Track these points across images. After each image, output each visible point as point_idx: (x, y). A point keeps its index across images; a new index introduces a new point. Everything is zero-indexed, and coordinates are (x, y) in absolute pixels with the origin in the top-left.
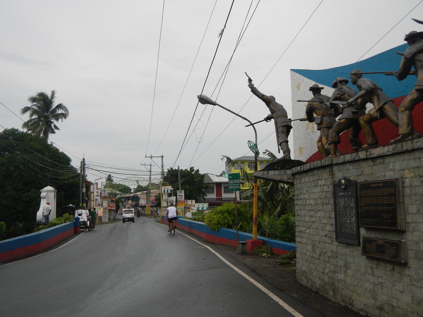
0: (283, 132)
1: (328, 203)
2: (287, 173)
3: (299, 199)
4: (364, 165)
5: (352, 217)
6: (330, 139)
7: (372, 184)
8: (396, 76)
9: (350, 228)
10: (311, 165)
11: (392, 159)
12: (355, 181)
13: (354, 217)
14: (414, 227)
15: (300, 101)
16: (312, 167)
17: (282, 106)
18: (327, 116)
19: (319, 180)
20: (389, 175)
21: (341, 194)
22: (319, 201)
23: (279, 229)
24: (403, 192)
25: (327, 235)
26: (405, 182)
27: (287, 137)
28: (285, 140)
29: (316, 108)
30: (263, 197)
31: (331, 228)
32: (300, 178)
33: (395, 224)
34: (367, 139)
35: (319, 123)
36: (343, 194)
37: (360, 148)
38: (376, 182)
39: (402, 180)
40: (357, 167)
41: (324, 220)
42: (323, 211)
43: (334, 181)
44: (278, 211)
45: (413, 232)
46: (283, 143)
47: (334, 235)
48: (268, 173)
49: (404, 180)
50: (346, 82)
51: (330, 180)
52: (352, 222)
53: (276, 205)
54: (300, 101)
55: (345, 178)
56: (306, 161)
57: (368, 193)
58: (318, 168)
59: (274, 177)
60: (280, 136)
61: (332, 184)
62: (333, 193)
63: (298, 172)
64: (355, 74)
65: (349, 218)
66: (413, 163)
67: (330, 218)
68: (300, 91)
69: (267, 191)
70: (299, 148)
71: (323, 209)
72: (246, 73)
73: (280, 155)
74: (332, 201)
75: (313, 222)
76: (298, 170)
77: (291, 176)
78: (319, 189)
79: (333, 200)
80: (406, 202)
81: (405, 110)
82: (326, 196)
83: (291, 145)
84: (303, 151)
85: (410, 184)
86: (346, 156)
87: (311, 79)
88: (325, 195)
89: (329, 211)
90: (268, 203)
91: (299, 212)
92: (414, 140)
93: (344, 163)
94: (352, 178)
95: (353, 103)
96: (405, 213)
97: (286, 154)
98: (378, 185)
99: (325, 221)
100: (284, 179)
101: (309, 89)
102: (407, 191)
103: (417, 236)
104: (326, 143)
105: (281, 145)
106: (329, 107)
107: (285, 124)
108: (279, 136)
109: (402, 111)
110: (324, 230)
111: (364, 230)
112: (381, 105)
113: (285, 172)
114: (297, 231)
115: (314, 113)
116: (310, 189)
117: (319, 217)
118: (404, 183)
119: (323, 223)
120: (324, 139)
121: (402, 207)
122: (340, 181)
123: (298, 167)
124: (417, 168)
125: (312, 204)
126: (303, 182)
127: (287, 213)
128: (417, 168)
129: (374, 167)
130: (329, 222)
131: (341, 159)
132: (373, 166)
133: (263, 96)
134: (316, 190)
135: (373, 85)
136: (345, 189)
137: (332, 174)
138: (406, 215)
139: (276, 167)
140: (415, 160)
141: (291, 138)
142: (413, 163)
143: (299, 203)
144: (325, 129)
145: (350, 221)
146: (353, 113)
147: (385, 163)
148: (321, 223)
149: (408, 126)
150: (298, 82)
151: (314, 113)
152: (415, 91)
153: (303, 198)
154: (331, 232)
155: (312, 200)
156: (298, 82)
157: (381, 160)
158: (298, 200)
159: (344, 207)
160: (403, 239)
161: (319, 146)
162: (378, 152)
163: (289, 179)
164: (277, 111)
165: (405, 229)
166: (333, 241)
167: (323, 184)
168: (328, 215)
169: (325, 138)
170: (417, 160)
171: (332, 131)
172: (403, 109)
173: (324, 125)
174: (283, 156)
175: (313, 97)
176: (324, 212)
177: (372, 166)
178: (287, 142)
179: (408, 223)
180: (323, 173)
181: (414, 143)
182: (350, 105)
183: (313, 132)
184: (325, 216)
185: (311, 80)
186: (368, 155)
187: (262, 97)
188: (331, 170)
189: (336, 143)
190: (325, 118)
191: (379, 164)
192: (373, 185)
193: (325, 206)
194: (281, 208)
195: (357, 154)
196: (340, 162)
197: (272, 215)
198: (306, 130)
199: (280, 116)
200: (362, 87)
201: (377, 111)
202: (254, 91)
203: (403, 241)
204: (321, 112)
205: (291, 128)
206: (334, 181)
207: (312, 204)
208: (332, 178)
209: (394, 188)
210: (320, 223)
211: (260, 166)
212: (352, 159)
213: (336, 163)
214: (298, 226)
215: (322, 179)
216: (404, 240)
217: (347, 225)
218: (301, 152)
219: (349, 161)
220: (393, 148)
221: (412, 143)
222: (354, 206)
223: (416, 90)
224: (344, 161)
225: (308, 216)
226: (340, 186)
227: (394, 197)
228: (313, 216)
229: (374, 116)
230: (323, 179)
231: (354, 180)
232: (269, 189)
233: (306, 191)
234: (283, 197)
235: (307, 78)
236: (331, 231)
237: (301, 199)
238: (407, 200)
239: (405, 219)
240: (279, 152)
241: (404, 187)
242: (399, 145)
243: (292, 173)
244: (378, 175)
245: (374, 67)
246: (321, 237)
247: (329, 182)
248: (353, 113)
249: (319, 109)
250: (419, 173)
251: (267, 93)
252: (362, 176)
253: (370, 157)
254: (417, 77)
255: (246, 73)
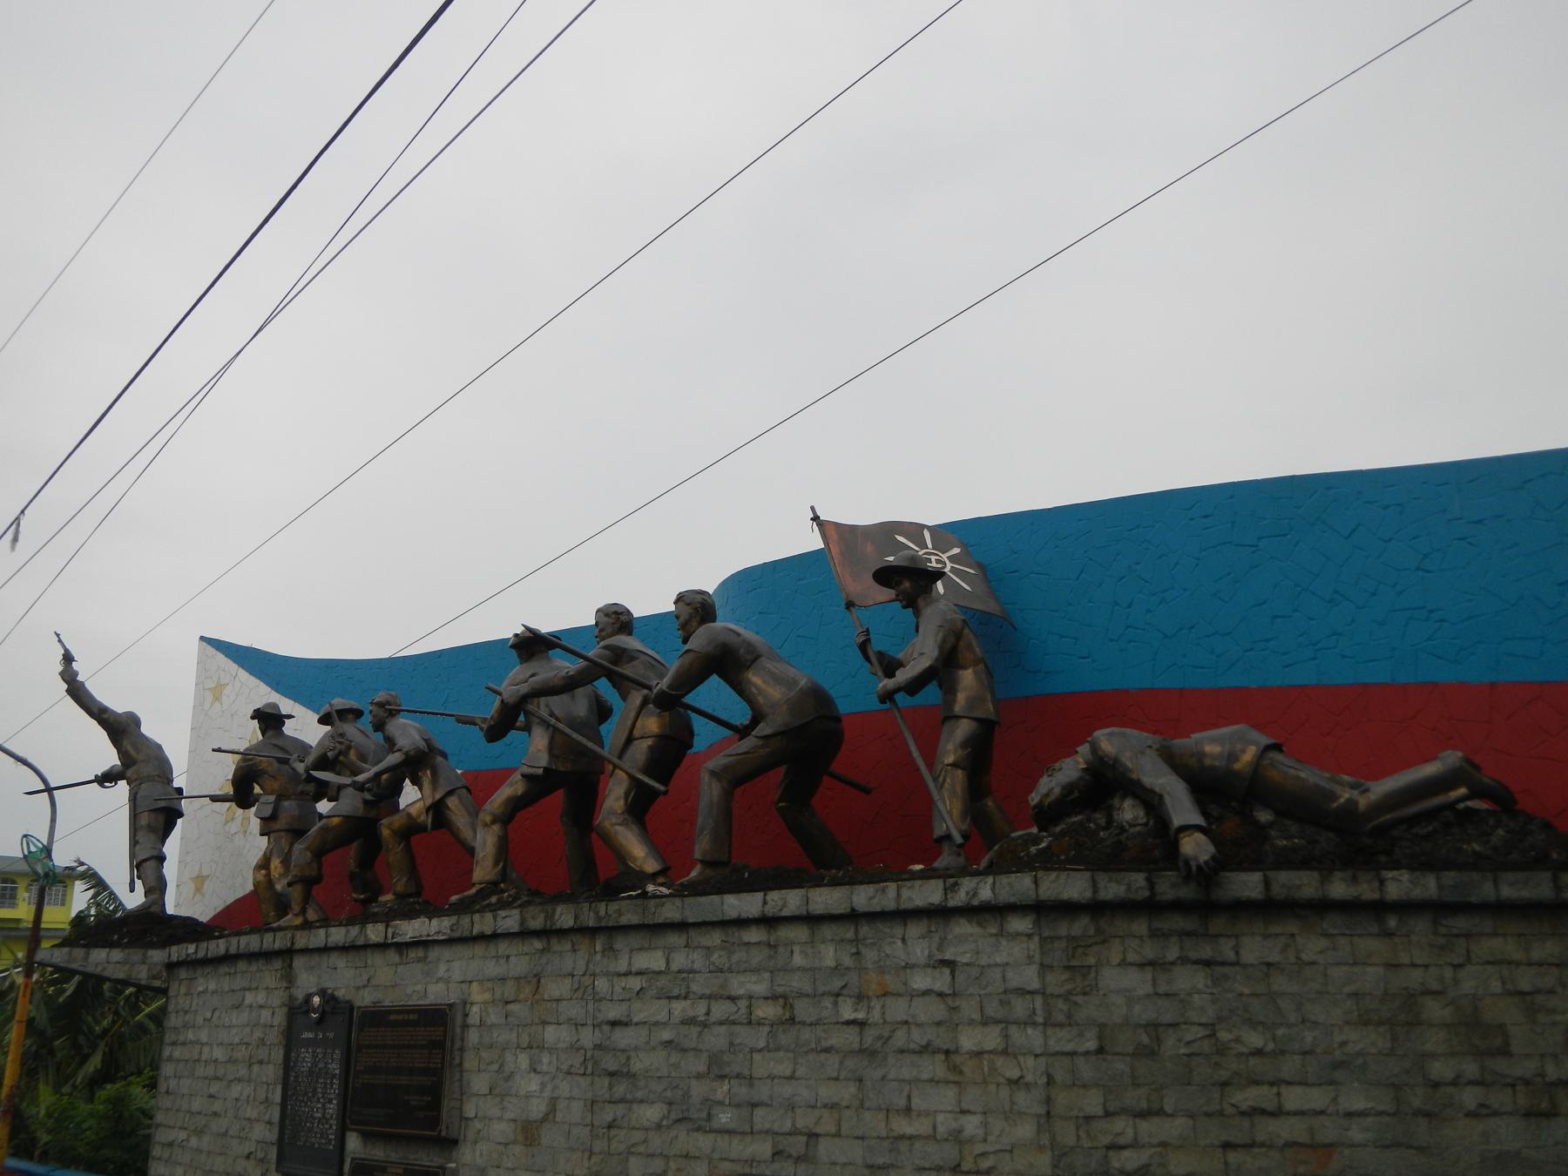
0: (150, 828)
1: (266, 1060)
2: (151, 957)
3: (179, 1042)
4: (376, 959)
5: (330, 1101)
6: (294, 872)
7: (389, 1012)
8: (481, 729)
9: (321, 1134)
10: (230, 944)
11: (446, 953)
12: (348, 1002)
13: (334, 1102)
14: (480, 1131)
15: (219, 750)
16: (233, 951)
17: (159, 747)
18: (293, 797)
19: (249, 989)
20: (436, 993)
21: (306, 1035)
22: (242, 1053)
23: (88, 1133)
24: (463, 1040)
25: (251, 1153)
26: (471, 1013)
27: (163, 843)
28: (155, 853)
29: (266, 773)
30: (42, 1019)
31: (267, 1133)
32: (191, 979)
33: (435, 1122)
34: (394, 881)
35: (267, 816)
36: (311, 1035)
37: (374, 904)
38: (399, 1010)
39: (464, 1007)
40: (359, 965)
41: (249, 1110)
42: (248, 1082)
43: (291, 997)
44: (91, 1069)
45: (476, 1142)
46: (148, 863)
47: (273, 1154)
48: (88, 954)
49: (467, 1009)
50: (358, 714)
51: (281, 993)
52: (328, 1116)
53: (86, 1051)
54: (219, 750)
55: (322, 992)
56: (209, 921)
57: (379, 1038)
58: (252, 957)
59: (104, 969)
60: (140, 841)
61: (286, 1005)
62: (284, 1030)
63: (189, 959)
64: (381, 705)
65: (319, 1106)
66: (493, 969)
67: (266, 1105)
68: (222, 704)
69: (61, 1000)
70: (195, 876)
71: (250, 1076)
72: (58, 635)
73: (133, 899)
74: (278, 1055)
75: (215, 1114)
76: (188, 955)
77: (163, 969)
78: (244, 1016)
79: (282, 1052)
80: (467, 1065)
81: (493, 822)
82: (263, 1039)
83: (170, 870)
84: (207, 886)
85: (481, 1021)
86: (333, 930)
87: (259, 678)
88: (261, 1036)
89: (266, 1083)
90: (60, 1041)
91: (173, 1083)
92: (499, 912)
93: (325, 950)
94: (340, 994)
95: (367, 786)
96: (462, 1094)
97: (154, 897)
98: (406, 1017)
99: (250, 1112)
100: (139, 977)
101: (250, 712)
102: (473, 1037)
103: (484, 1152)
104: (280, 875)
105: (141, 869)
106: (303, 778)
107: (162, 804)
108: (137, 838)
109: (486, 825)
110: (246, 1138)
111: (358, 1137)
112: (438, 796)
113: (145, 956)
114: (159, 1143)
115: (256, 785)
116: (217, 1014)
117: (236, 1099)
118: (466, 1015)
119: (245, 1119)
120: (276, 863)
121: (457, 1076)
122: (308, 998)
123: (189, 946)
124: (499, 980)
125: (220, 1060)
126: (200, 992)
127: (125, 1078)
128: (499, 980)
129: (400, 969)
130: (264, 1114)
131: (318, 938)
132: (400, 964)
133: (104, 710)
134: (237, 1018)
135: (424, 740)
136: (320, 1021)
137: (289, 978)
138: (465, 1098)
139: (116, 937)
140: (497, 961)
141: (172, 846)
142: (493, 969)
143: (177, 1053)
144: (283, 834)
145: (324, 1114)
146: (366, 802)
147: (428, 960)
148: (240, 1119)
149: (496, 864)
150: (219, 678)
151: (256, 785)
152: (520, 777)
153: (191, 1040)
154: (264, 1145)
155: (220, 1046)
156: (219, 678)
157: (420, 953)
158: (174, 1044)
159: (311, 1072)
160: (450, 1161)
161: (259, 882)
162: (414, 930)
163: (154, 977)
164: (143, 761)
165: (459, 1135)
166: (267, 1171)
167: (259, 1003)
168: (261, 1095)
169: (281, 862)
170: (502, 961)
171: (302, 846)
172: (488, 819)
173: (282, 823)
174: (143, 904)
175: (261, 737)
176: (253, 1085)
177: (396, 965)
178: (161, 859)
179: (467, 1119)
180: (262, 971)
181: (499, 919)
182: (360, 787)
183: (245, 832)
184: (254, 1097)
185: (258, 681)
186: (390, 935)
187: (101, 715)
188: (286, 965)
189: (309, 883)
190: (286, 803)
191: (413, 962)
192: (393, 1017)
193: (256, 1068)
194: (103, 1061)
195: (362, 930)
196: (316, 946)
197: (67, 1082)
198: (225, 825)
199: (149, 778)
200: (396, 742)
201: (428, 810)
202: (77, 692)
203: (450, 1168)
204: (276, 785)
205: (181, 815)
206: (291, 997)
207: (220, 1060)
208: (286, 988)
209: (441, 1029)
210: (236, 1117)
211: (26, 895)
212: (348, 941)
213: (303, 947)
214: (165, 1126)
215: (257, 988)
216: (453, 1165)
217: (313, 1124)
218: (198, 890)
219: (341, 944)
220: (451, 924)
221: (495, 918)
222: (337, 1072)
223: (523, 776)
224: (326, 944)
225: (202, 1096)
226: (307, 1012)
227: (441, 1052)
228: (216, 1095)
229: (419, 820)
230: (260, 988)
231: (347, 998)
232: (68, 993)
233: (205, 1019)
234: (114, 1022)
235: (247, 671)
236: (266, 1143)
237: (184, 1044)
238: (470, 1062)
239: (461, 1109)
240: (132, 890)
241: (465, 1026)
242: (466, 920)
243: (167, 961)
244: (409, 991)
245: (437, 680)
246: (234, 1161)
247: (278, 998)
248: (366, 802)
249: (274, 777)
250: (503, 993)
251: (118, 704)
252: (367, 990)
253: (395, 940)
254: (530, 735)
255: (58, 635)
